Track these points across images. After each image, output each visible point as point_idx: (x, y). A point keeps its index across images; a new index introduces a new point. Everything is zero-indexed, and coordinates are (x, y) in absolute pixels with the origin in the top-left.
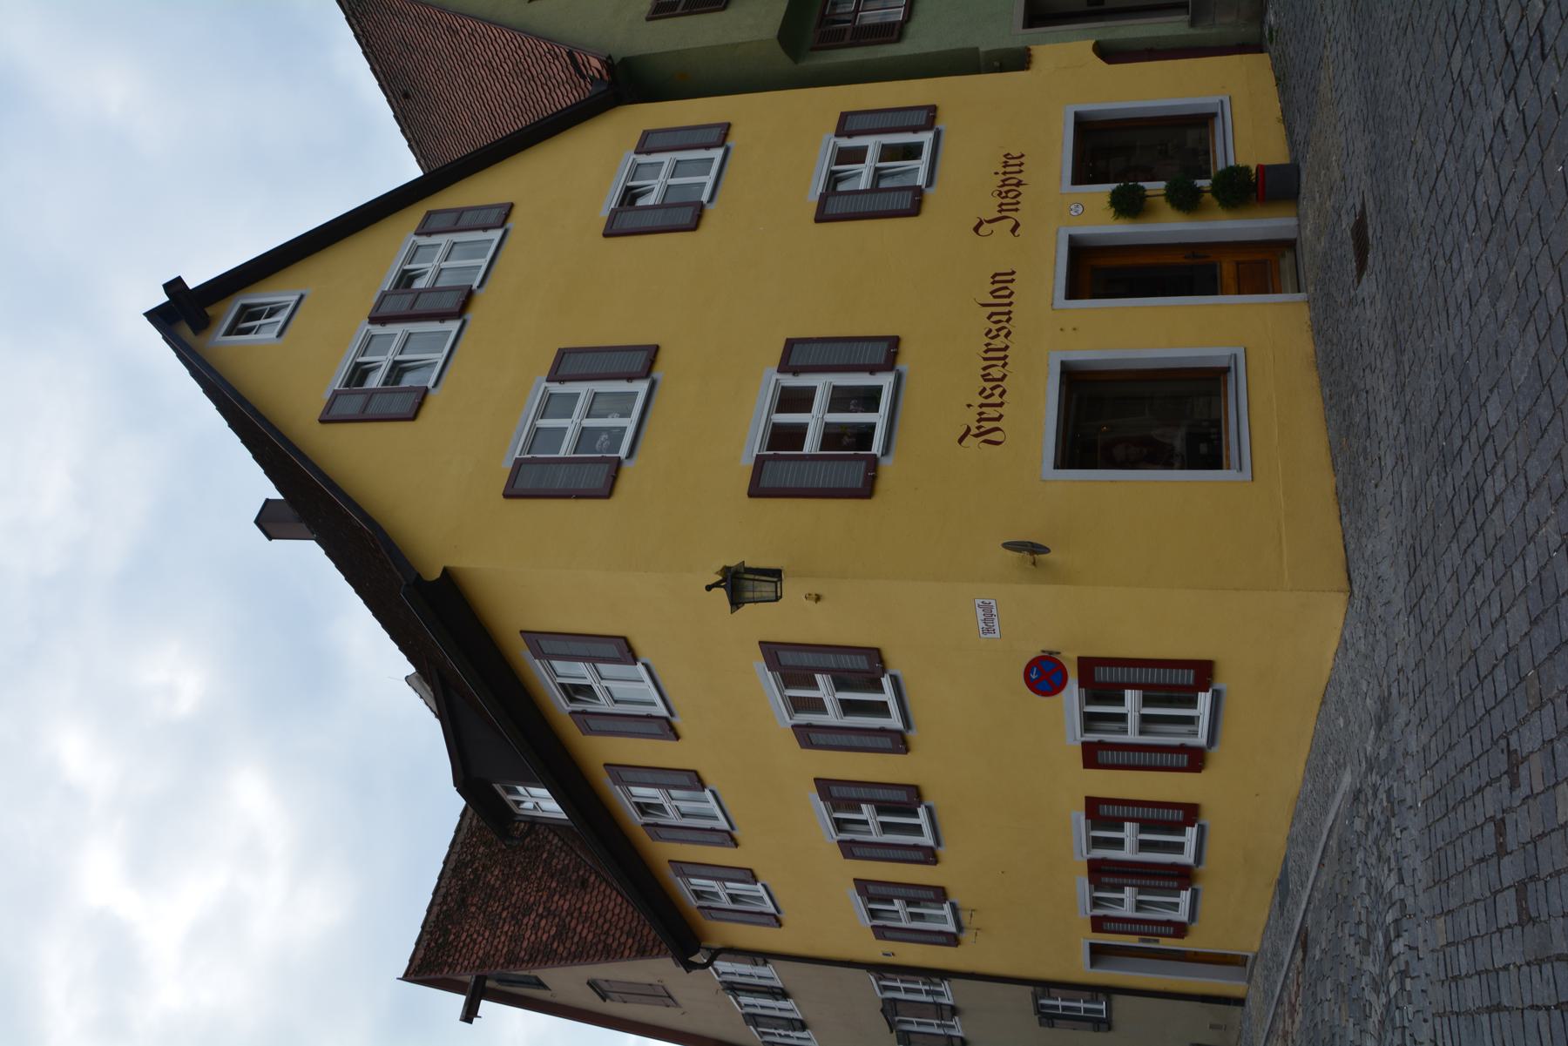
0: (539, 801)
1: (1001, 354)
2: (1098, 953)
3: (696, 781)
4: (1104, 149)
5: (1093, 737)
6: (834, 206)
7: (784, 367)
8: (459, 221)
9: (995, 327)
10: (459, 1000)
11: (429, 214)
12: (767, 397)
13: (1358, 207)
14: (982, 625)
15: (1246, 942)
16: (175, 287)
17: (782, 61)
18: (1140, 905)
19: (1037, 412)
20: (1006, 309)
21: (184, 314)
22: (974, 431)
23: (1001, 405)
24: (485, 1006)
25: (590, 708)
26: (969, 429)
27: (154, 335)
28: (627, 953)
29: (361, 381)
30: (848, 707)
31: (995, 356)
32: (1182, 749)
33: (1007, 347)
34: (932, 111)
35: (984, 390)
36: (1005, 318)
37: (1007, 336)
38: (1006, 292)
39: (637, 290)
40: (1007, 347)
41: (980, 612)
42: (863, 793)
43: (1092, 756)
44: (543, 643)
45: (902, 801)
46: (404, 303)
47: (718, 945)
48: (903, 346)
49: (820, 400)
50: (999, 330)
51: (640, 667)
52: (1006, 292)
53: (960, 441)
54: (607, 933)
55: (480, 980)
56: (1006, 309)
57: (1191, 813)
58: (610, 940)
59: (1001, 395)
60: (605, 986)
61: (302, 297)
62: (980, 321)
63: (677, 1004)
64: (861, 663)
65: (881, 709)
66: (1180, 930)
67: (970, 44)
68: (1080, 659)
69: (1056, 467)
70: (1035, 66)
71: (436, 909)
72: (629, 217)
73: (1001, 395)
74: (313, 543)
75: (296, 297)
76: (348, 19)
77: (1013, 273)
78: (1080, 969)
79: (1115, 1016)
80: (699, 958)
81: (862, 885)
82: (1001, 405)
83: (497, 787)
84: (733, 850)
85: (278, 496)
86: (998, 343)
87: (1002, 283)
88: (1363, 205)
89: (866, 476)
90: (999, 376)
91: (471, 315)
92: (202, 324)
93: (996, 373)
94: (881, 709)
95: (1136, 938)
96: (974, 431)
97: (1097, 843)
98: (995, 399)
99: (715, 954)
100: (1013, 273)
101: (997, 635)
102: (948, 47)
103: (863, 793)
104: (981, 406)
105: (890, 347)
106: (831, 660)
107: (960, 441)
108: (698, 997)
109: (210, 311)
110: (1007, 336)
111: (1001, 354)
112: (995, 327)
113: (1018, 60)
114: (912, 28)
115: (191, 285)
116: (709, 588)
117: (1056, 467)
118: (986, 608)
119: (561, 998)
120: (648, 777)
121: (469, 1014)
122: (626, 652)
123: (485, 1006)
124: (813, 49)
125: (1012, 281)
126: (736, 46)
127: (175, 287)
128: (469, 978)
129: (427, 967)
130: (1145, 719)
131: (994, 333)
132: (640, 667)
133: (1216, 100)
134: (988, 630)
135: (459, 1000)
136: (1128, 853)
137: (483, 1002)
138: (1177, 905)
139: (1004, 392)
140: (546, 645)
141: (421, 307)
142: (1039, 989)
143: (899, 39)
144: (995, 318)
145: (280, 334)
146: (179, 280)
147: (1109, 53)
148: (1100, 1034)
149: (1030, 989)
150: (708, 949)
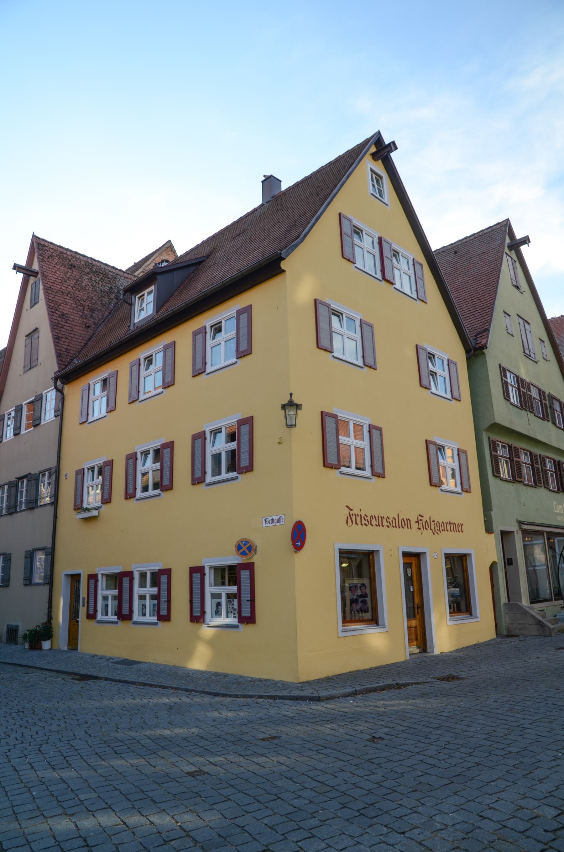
0: (145, 308)
1: (380, 524)
2: (75, 578)
3: (168, 384)
4: (458, 565)
5: (207, 571)
6: (432, 448)
7: (371, 428)
8: (417, 279)
9: (390, 520)
10: (23, 263)
11: (421, 265)
12: (360, 420)
13: (462, 677)
14: (270, 518)
15: (84, 646)
16: (393, 146)
17: (486, 424)
18: (142, 597)
19: (360, 539)
20: (397, 526)
21: (381, 149)
22: (351, 512)
23: (362, 524)
24: (20, 276)
25: (208, 336)
26: (352, 510)
27: (369, 134)
28: (58, 348)
29: (355, 232)
30: (217, 458)
31: (379, 521)
32: (96, 611)
33: (383, 526)
34: (468, 491)
35: (367, 516)
36: (394, 525)
37: (387, 526)
38: (403, 525)
39: (397, 360)
40: (383, 526)
41: (278, 517)
42: (167, 464)
43: (197, 571)
44: (246, 315)
45: (164, 484)
46: (384, 252)
47: (65, 392)
48: (381, 479)
49: (359, 443)
50: (367, 520)
51: (234, 360)
52: (403, 525)
53: (347, 506)
54: (66, 338)
55: (35, 274)
56: (397, 526)
57: (165, 618)
58: (63, 340)
59: (365, 524)
60: (36, 336)
61: (387, 205)
62: (392, 515)
63: (25, 372)
64: (244, 462)
65: (217, 471)
66: (92, 616)
67: (494, 507)
68: (254, 563)
69: (445, 554)
70: (487, 535)
71: (51, 246)
72: (423, 356)
73: (365, 524)
74: (260, 202)
75: (387, 203)
76: (491, 227)
77: (411, 528)
78: (63, 570)
79: (33, 587)
80: (59, 383)
81: (110, 463)
82: (362, 524)
83: (152, 288)
84: (127, 401)
85: (284, 187)
86: (385, 523)
87: (457, 527)
88: (463, 679)
89: (332, 464)
90: (372, 523)
91: (384, 283)
92: (375, 156)
93: (374, 522)
94: (217, 471)
95: (85, 596)
96: (351, 512)
97: (143, 576)
98: (363, 522)
99: (60, 391)
100: (411, 528)
101: (264, 525)
102: (492, 497)
103: (167, 464)
104: (361, 515)
105: (381, 474)
106: (245, 449)
107: (347, 506)
108: (34, 380)
109: (380, 161)
110: (387, 526)
111: (380, 524)
112: (390, 520)
113: (489, 529)
114: (498, 481)
115: (392, 154)
116: (291, 394)
117: (445, 554)
118: (280, 520)
119: (24, 313)
120: (169, 362)
121: (17, 268)
122: (243, 352)
123: (20, 276)
124: (489, 438)
125: (408, 528)
126: (492, 405)
127: (393, 146)
128: (36, 267)
129: (39, 246)
130: (219, 596)
131: (388, 520)
132: (234, 360)
133: (478, 615)
134: (267, 521)
135: (23, 263)
136: (137, 590)
137: (22, 275)
138: (107, 614)
139: (366, 525)
140: (244, 317)
141: (386, 260)
142: (50, 550)
143: (494, 475)
144: (394, 520)
145: (372, 194)
146: (396, 148)
147: (493, 568)
148: (22, 580)
149: (50, 545)
150: (63, 388)
